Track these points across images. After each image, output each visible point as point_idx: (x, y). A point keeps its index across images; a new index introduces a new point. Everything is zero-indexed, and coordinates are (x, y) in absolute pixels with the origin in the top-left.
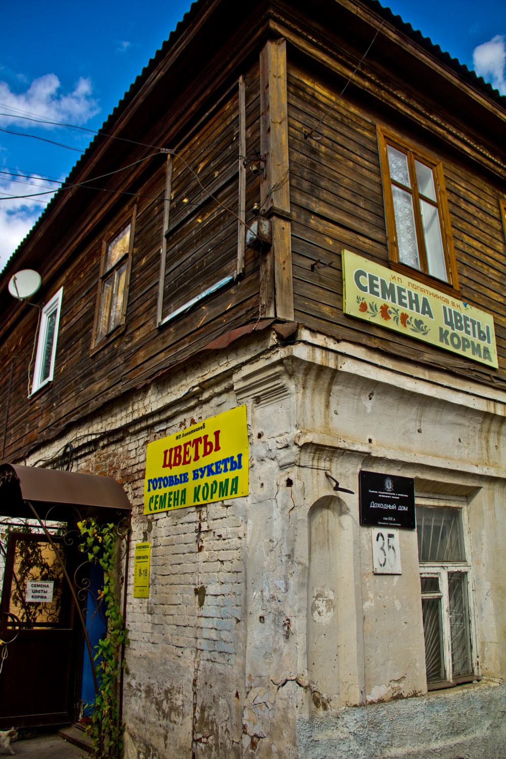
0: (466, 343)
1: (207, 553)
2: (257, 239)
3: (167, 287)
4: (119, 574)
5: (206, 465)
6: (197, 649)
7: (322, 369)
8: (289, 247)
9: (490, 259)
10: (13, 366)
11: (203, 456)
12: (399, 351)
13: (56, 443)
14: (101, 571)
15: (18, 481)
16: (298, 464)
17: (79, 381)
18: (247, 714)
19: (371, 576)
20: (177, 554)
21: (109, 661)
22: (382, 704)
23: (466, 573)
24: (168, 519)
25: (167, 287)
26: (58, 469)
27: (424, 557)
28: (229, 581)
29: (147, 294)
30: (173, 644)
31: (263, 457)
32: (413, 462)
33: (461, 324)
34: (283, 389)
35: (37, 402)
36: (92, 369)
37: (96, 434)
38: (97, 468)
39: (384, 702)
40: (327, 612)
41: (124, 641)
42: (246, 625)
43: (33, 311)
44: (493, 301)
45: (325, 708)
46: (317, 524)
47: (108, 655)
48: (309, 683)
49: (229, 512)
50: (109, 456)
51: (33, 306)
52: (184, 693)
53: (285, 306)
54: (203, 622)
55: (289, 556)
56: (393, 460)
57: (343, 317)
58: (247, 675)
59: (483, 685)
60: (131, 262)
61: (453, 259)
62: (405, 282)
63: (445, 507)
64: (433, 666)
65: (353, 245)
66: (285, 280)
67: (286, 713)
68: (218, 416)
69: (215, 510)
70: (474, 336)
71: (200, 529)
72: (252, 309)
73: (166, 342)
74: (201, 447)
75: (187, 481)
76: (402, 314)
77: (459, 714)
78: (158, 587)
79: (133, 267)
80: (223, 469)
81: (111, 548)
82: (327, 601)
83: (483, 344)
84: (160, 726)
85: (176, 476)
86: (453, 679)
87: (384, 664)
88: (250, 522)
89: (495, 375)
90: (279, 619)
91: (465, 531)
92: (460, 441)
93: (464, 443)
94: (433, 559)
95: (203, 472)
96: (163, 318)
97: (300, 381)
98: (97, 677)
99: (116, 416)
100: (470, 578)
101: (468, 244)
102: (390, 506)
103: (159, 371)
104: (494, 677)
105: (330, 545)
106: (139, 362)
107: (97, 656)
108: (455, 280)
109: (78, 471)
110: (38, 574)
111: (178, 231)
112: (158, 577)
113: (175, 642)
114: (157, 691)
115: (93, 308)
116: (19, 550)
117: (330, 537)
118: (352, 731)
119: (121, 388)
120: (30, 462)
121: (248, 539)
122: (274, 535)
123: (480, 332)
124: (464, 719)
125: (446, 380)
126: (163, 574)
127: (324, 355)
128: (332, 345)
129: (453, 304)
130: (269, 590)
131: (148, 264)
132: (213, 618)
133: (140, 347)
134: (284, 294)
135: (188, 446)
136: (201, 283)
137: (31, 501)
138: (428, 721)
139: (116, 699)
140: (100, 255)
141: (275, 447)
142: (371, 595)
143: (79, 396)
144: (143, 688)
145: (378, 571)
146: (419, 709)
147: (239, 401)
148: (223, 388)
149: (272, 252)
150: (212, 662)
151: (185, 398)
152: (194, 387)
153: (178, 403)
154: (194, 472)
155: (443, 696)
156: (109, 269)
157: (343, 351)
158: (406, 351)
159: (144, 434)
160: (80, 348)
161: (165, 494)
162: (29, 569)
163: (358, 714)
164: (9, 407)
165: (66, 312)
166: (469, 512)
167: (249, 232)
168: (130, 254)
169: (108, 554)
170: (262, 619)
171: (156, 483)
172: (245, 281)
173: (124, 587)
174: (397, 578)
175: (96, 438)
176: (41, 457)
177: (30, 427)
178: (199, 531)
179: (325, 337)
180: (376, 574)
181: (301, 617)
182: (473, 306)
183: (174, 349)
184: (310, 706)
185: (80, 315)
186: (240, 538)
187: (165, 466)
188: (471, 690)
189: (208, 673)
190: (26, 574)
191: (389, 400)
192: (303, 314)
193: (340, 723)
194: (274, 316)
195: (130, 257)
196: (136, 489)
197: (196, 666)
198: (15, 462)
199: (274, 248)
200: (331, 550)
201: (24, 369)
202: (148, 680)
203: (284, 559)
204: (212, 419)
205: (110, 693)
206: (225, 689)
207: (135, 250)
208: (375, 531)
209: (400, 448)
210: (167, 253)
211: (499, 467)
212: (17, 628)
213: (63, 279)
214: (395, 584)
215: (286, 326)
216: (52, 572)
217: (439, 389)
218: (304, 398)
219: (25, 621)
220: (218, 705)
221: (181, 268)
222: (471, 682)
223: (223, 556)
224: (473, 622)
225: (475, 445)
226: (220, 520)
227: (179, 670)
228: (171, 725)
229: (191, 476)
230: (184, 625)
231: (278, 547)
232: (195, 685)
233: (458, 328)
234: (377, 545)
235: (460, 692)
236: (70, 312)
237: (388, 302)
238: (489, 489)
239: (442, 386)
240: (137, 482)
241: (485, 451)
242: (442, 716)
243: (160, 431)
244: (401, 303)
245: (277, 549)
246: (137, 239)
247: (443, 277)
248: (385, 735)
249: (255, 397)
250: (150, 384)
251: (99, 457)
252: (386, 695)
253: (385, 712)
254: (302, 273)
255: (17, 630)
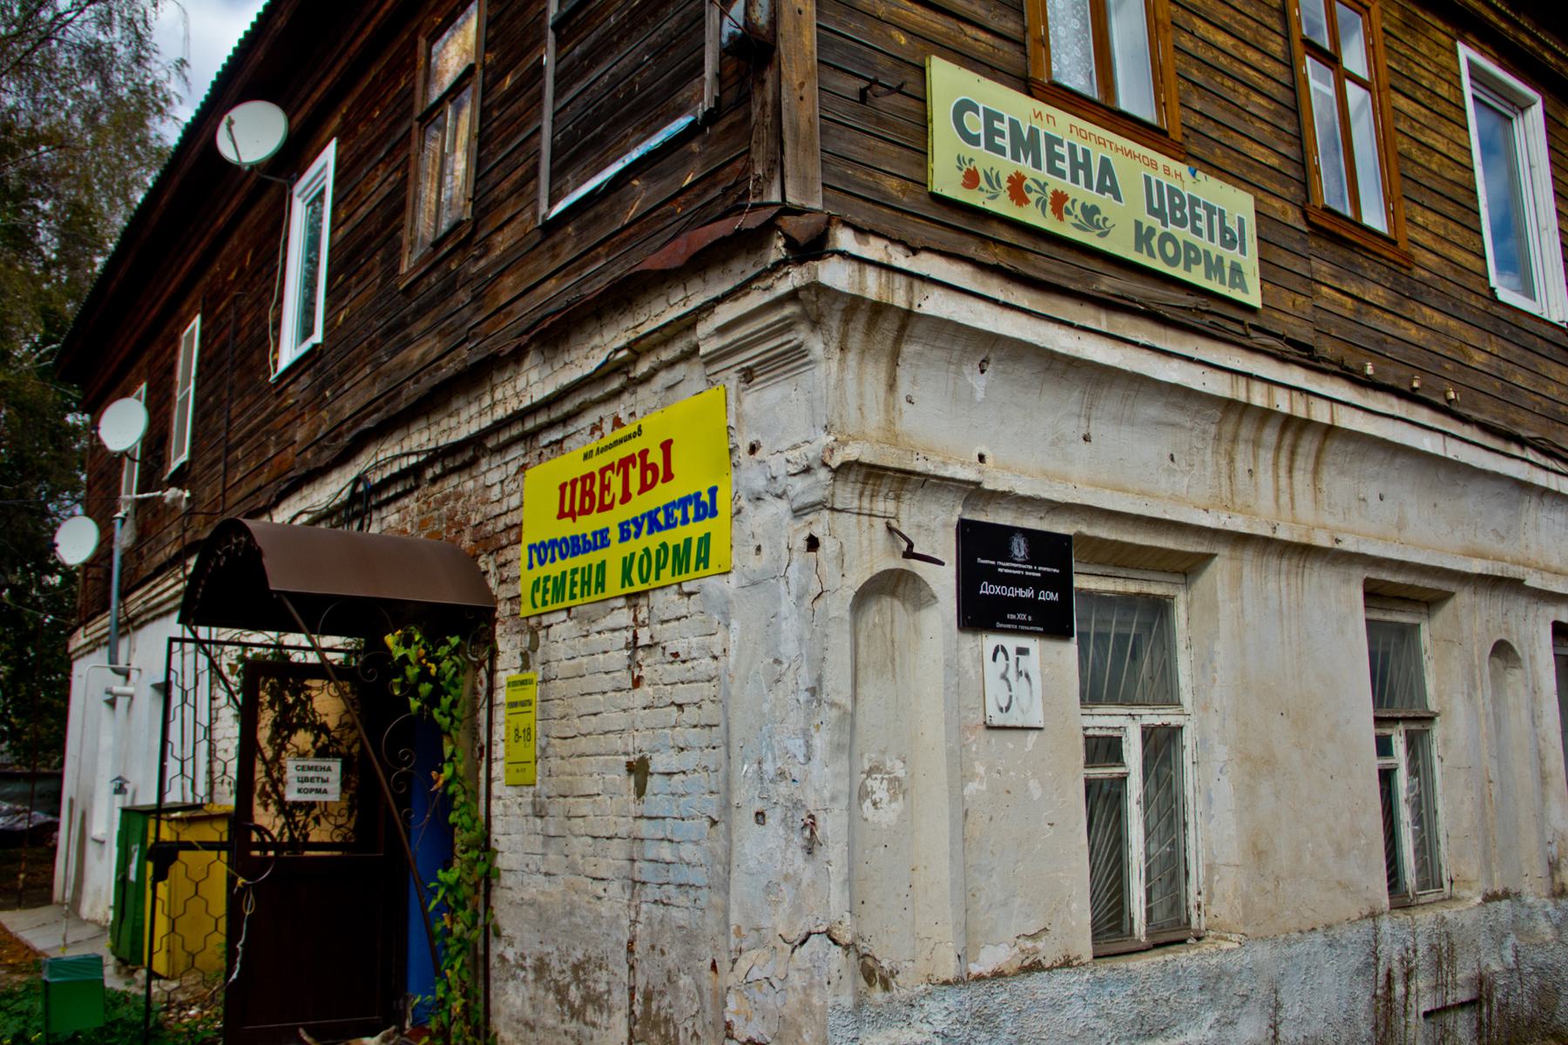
0: (1193, 254)
1: (650, 690)
2: (744, 35)
3: (558, 137)
4: (474, 739)
5: (645, 511)
6: (635, 882)
7: (879, 309)
8: (812, 53)
9: (1252, 73)
10: (236, 314)
11: (640, 492)
12: (1046, 271)
13: (335, 475)
14: (436, 734)
15: (259, 553)
16: (829, 505)
17: (378, 342)
18: (733, 1002)
19: (981, 731)
20: (590, 694)
21: (460, 913)
22: (1001, 981)
23: (1181, 728)
24: (570, 623)
25: (558, 137)
26: (340, 529)
27: (1092, 695)
28: (695, 744)
29: (516, 155)
30: (587, 873)
31: (759, 493)
32: (1070, 501)
33: (1183, 215)
34: (798, 353)
35: (291, 389)
36: (404, 317)
37: (417, 453)
38: (423, 525)
39: (1005, 976)
40: (890, 802)
41: (488, 871)
42: (729, 830)
43: (273, 191)
44: (1257, 165)
45: (886, 987)
46: (871, 625)
47: (456, 901)
48: (854, 938)
49: (693, 605)
50: (446, 498)
51: (272, 182)
52: (610, 967)
53: (804, 179)
54: (645, 828)
55: (813, 691)
56: (1029, 497)
57: (929, 200)
58: (733, 928)
59: (1206, 947)
60: (480, 85)
61: (1170, 74)
62: (1062, 124)
63: (1138, 594)
64: (1109, 911)
65: (952, 45)
66: (804, 125)
67: (807, 995)
68: (668, 410)
69: (665, 602)
70: (1211, 239)
71: (635, 643)
72: (736, 184)
73: (558, 256)
74: (635, 473)
75: (608, 545)
76: (1055, 193)
77: (1155, 1001)
78: (554, 763)
79: (485, 95)
80: (680, 519)
81: (456, 687)
82: (890, 781)
83: (1231, 256)
84: (566, 1033)
85: (584, 536)
86: (1148, 935)
87: (1005, 904)
88: (735, 624)
89: (1254, 322)
90: (793, 816)
91: (1181, 645)
92: (1172, 459)
93: (1181, 463)
94: (1114, 698)
95: (639, 527)
96: (551, 204)
97: (835, 334)
98: (437, 943)
99: (459, 414)
100: (1188, 739)
101: (1203, 40)
102: (1021, 591)
103: (544, 317)
104: (1230, 932)
105: (898, 670)
106: (504, 299)
107: (434, 903)
108: (1173, 117)
109: (382, 531)
110: (309, 746)
111: (580, 17)
112: (553, 741)
113: (590, 870)
114: (558, 968)
115: (403, 184)
116: (268, 698)
117: (897, 653)
118: (939, 1029)
119: (467, 355)
120: (282, 515)
121: (732, 660)
122: (782, 650)
123: (1224, 230)
124: (1165, 1008)
125: (1143, 332)
126: (563, 735)
127: (883, 280)
128: (900, 259)
129: (1167, 171)
130: (774, 759)
131: (516, 90)
132: (664, 818)
133: (508, 265)
134: (801, 154)
135: (609, 473)
136: (630, 130)
137: (287, 594)
138: (1091, 1013)
139: (476, 987)
140: (414, 69)
141: (783, 472)
142: (980, 769)
143: (380, 374)
144: (529, 962)
145: (996, 722)
146: (1075, 990)
147: (711, 378)
148: (678, 352)
149: (776, 62)
150: (665, 904)
151: (599, 373)
152: (617, 351)
153: (586, 384)
154: (621, 525)
155: (1123, 965)
156: (435, 94)
157: (924, 272)
158: (1062, 272)
159: (517, 451)
160: (377, 272)
161: (564, 574)
162: (289, 737)
163: (951, 999)
164: (231, 401)
165: (345, 192)
166: (1189, 607)
167: (726, 20)
168: (478, 67)
169: (450, 698)
170: (760, 816)
171: (544, 551)
172: (721, 126)
173: (484, 765)
174: (1033, 735)
175: (418, 463)
176: (303, 505)
177: (277, 444)
178: (633, 645)
179: (886, 242)
180: (990, 728)
181: (837, 811)
182: (1212, 175)
183: (576, 270)
184: (855, 982)
185: (375, 200)
186: (715, 658)
187: (561, 515)
188: (1183, 954)
189: (657, 927)
190: (282, 747)
191: (1023, 372)
192: (842, 195)
193: (916, 1015)
194: (780, 201)
195: (479, 72)
196: (504, 565)
197: (633, 914)
198: (255, 514)
199: (780, 56)
200: (898, 679)
201: (260, 320)
202: (538, 946)
203: (803, 697)
204: (657, 416)
205: (464, 975)
206: (690, 955)
207: (490, 58)
208: (990, 641)
209: (1045, 473)
210: (557, 63)
211: (1255, 514)
212: (271, 853)
213: (336, 122)
214: (1030, 747)
215: (803, 220)
216: (338, 742)
217: (1130, 351)
218: (842, 369)
219: (286, 839)
220: (677, 989)
221: (586, 97)
222: (1183, 941)
223: (682, 694)
224: (1191, 826)
225: (1205, 469)
226: (676, 623)
227: (600, 925)
228: (587, 1030)
229: (614, 535)
230: (607, 835)
231: (790, 674)
232: (630, 951)
233: (1176, 222)
234: (993, 670)
235: (1160, 959)
236: (354, 193)
237: (1025, 166)
238: (1231, 558)
239: (1135, 344)
240: (505, 551)
241: (1225, 481)
242: (1121, 1004)
243: (551, 443)
244: (1053, 170)
245: (789, 679)
246: (491, 34)
247: (1148, 113)
248: (1004, 1037)
249: (743, 369)
250: (528, 345)
251: (425, 502)
252: (1008, 962)
253: (1006, 996)
254: (840, 108)
255: (270, 857)
